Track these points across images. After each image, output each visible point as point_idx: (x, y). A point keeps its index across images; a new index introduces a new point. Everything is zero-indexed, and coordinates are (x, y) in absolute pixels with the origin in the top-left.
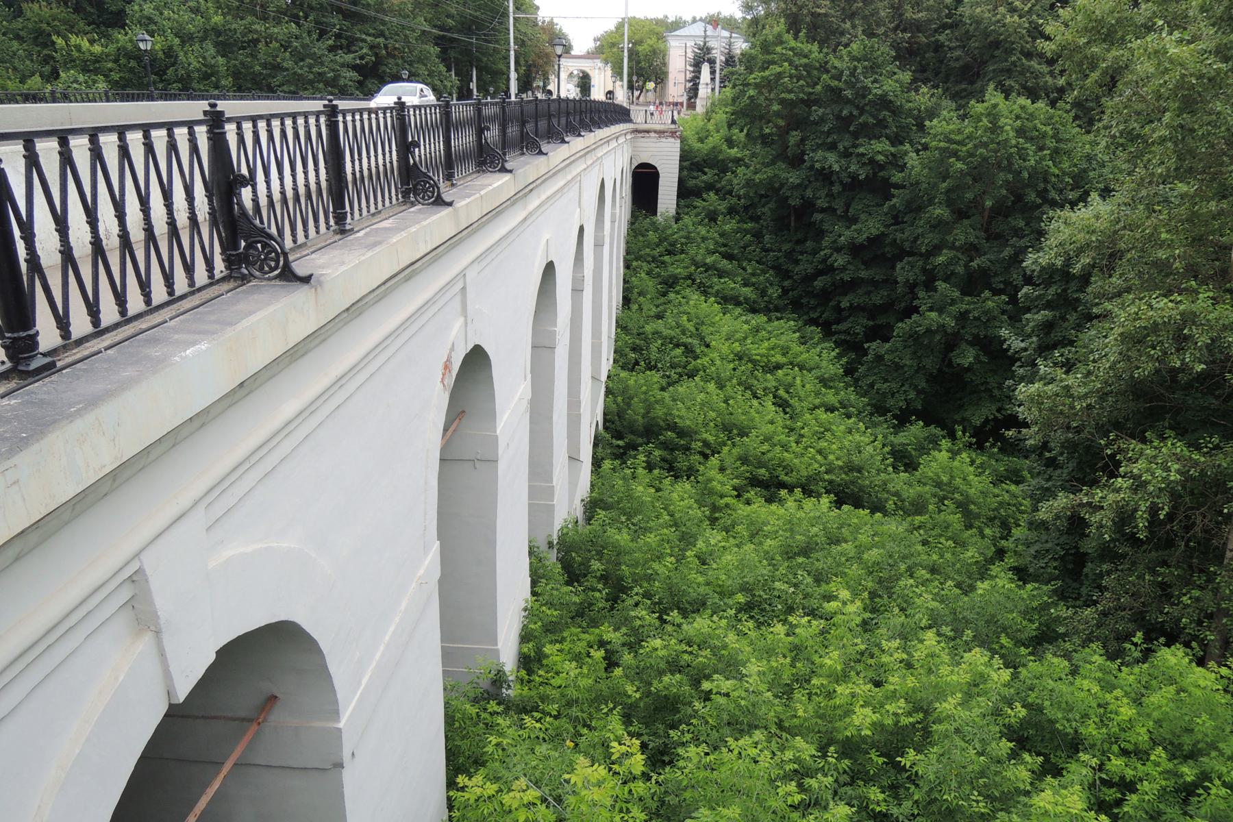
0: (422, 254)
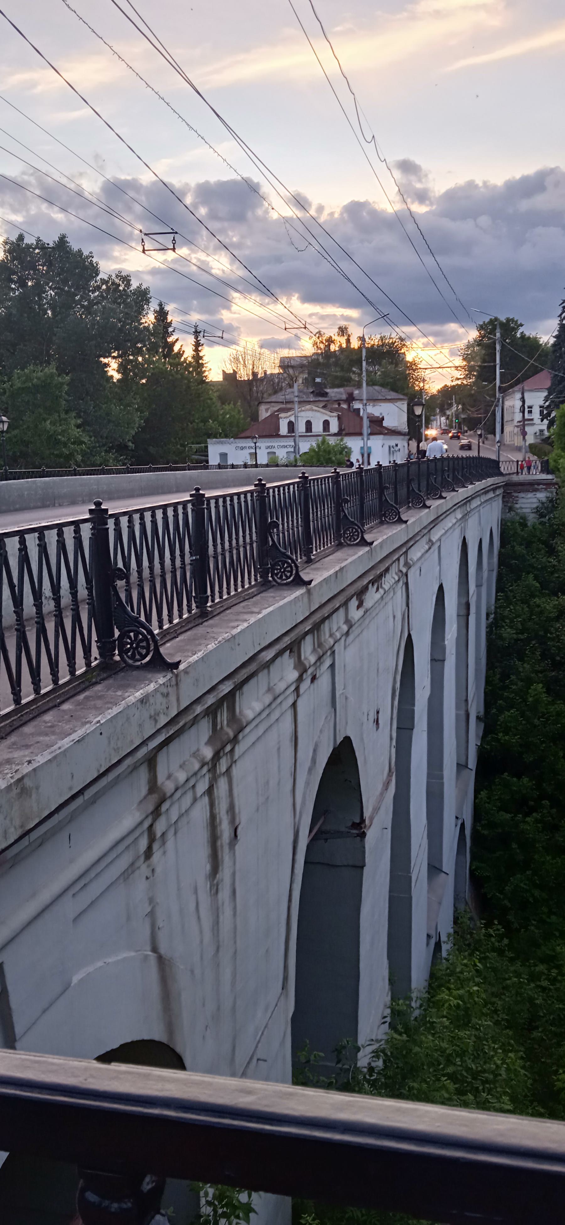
0: (460, 500)
